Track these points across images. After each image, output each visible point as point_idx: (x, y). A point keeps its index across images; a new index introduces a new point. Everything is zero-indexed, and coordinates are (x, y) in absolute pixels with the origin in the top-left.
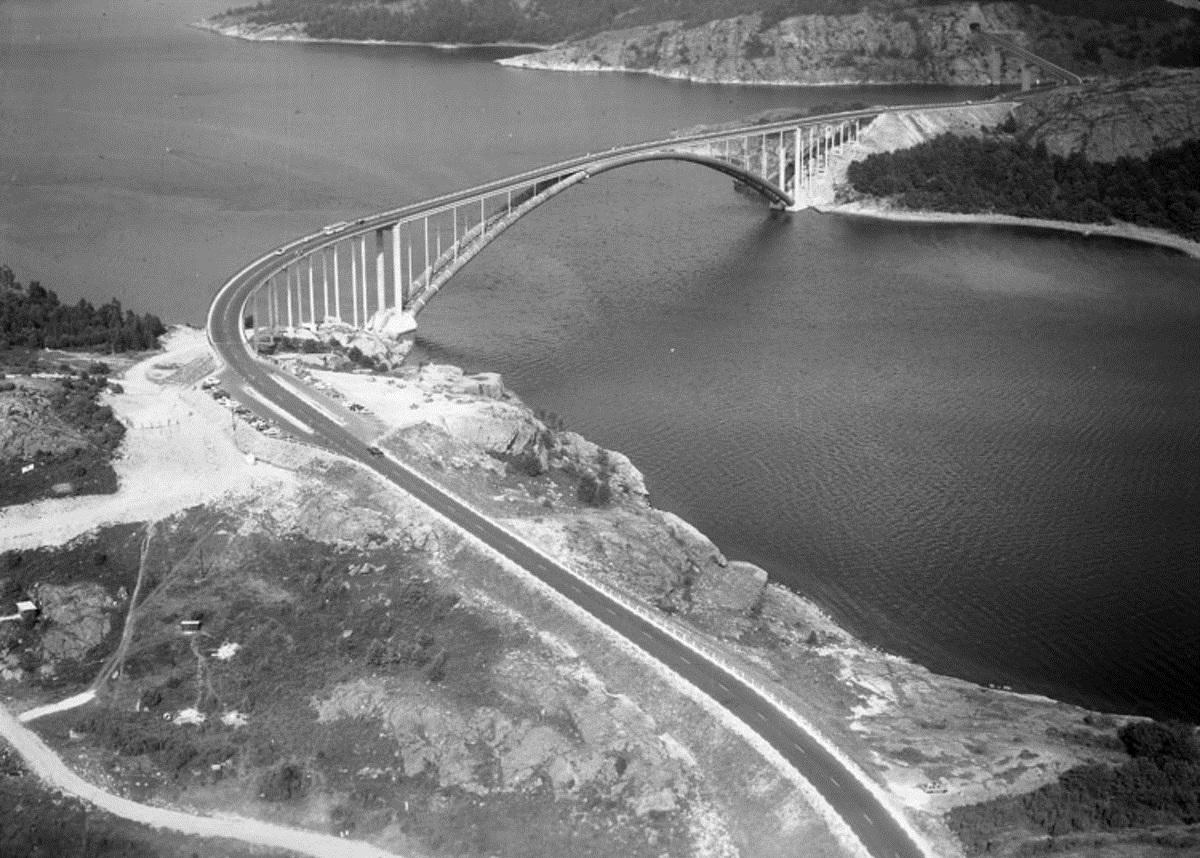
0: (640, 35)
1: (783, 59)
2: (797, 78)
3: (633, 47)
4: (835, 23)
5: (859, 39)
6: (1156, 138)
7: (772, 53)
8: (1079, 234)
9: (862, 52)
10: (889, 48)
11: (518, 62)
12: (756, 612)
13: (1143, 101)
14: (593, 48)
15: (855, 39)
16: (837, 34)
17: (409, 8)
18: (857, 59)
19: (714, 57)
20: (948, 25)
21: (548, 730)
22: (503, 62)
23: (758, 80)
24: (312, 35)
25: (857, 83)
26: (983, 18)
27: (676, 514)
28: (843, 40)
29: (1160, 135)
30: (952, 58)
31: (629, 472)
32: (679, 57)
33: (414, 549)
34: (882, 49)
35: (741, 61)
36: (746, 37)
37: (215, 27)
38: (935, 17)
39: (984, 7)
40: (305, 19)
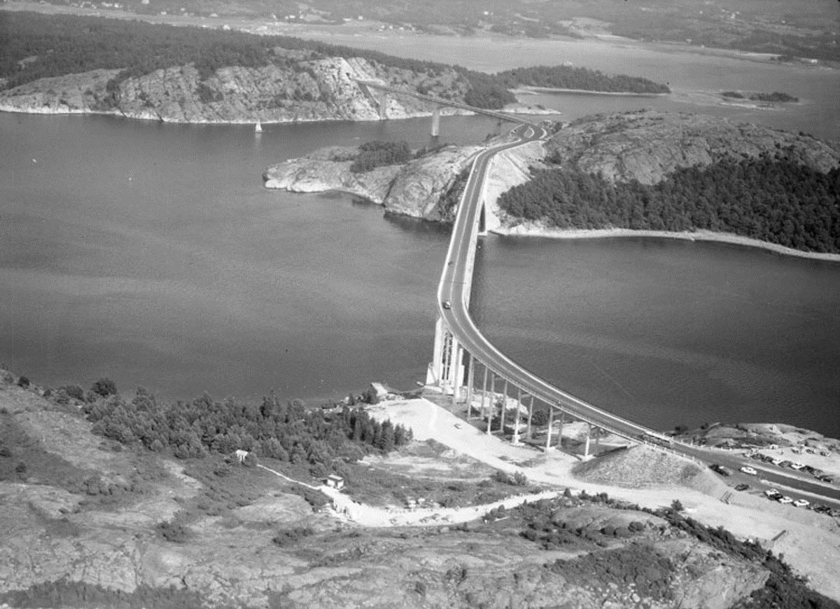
9: (284, 96)
15: (276, 85)
16: (262, 82)
19: (174, 101)
20: (336, 74)
25: (291, 120)
26: (351, 69)
30: (350, 100)
34: (297, 92)
39: (349, 60)
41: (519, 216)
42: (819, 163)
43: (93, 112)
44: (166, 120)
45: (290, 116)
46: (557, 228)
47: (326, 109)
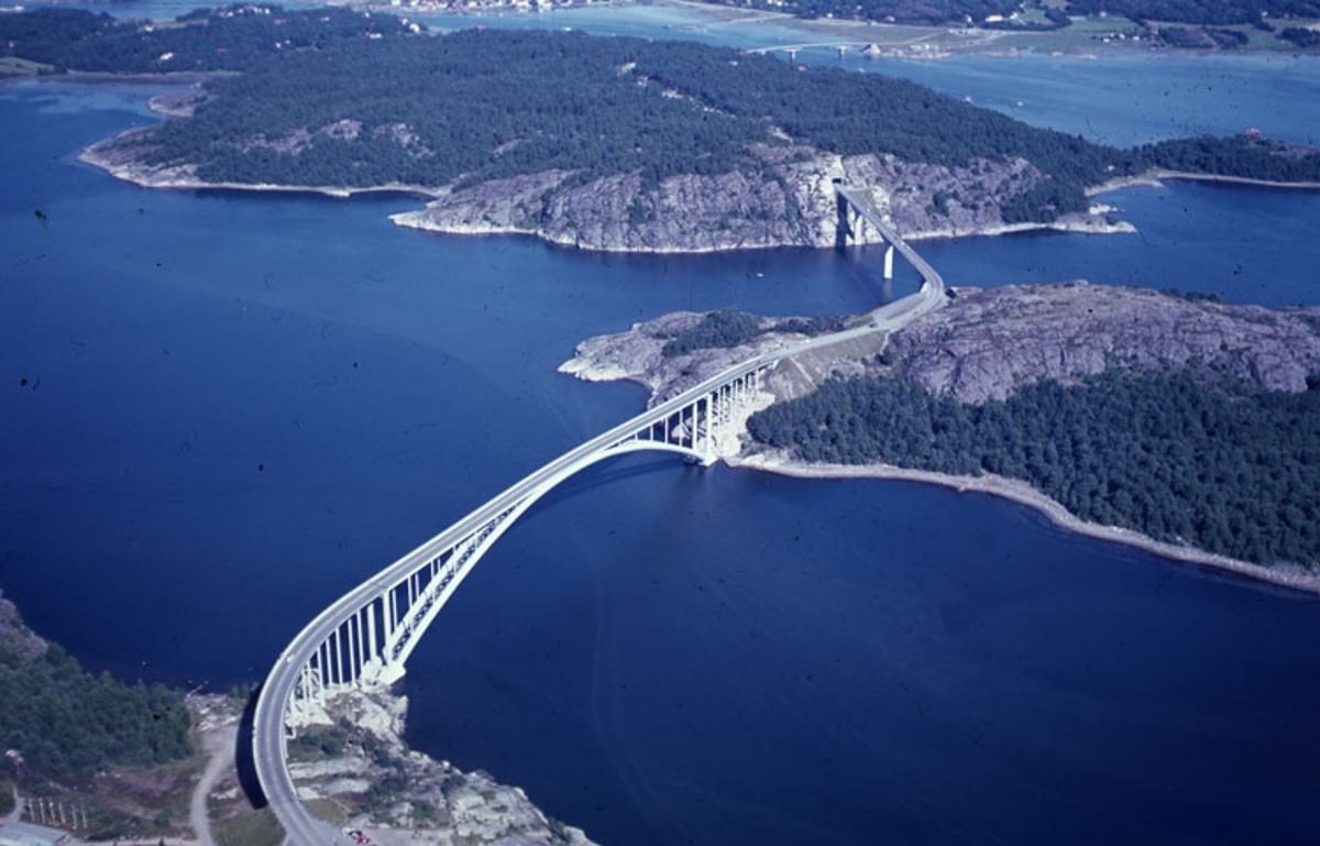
1: (664, 223)
2: (679, 244)
3: (520, 205)
4: (711, 184)
5: (733, 201)
6: (1015, 375)
7: (652, 217)
9: (735, 214)
13: (1003, 336)
14: (482, 205)
15: (729, 200)
18: (732, 221)
20: (813, 185)
22: (398, 219)
23: (643, 247)
24: (203, 179)
28: (723, 202)
29: (1019, 371)
30: (818, 219)
32: (566, 219)
34: (753, 209)
35: (626, 227)
36: (629, 201)
37: (104, 164)
38: (801, 175)
40: (197, 160)
41: (763, 442)
42: (1268, 376)
43: (519, 231)
44: (582, 245)
45: (733, 240)
46: (803, 460)
47: (784, 231)
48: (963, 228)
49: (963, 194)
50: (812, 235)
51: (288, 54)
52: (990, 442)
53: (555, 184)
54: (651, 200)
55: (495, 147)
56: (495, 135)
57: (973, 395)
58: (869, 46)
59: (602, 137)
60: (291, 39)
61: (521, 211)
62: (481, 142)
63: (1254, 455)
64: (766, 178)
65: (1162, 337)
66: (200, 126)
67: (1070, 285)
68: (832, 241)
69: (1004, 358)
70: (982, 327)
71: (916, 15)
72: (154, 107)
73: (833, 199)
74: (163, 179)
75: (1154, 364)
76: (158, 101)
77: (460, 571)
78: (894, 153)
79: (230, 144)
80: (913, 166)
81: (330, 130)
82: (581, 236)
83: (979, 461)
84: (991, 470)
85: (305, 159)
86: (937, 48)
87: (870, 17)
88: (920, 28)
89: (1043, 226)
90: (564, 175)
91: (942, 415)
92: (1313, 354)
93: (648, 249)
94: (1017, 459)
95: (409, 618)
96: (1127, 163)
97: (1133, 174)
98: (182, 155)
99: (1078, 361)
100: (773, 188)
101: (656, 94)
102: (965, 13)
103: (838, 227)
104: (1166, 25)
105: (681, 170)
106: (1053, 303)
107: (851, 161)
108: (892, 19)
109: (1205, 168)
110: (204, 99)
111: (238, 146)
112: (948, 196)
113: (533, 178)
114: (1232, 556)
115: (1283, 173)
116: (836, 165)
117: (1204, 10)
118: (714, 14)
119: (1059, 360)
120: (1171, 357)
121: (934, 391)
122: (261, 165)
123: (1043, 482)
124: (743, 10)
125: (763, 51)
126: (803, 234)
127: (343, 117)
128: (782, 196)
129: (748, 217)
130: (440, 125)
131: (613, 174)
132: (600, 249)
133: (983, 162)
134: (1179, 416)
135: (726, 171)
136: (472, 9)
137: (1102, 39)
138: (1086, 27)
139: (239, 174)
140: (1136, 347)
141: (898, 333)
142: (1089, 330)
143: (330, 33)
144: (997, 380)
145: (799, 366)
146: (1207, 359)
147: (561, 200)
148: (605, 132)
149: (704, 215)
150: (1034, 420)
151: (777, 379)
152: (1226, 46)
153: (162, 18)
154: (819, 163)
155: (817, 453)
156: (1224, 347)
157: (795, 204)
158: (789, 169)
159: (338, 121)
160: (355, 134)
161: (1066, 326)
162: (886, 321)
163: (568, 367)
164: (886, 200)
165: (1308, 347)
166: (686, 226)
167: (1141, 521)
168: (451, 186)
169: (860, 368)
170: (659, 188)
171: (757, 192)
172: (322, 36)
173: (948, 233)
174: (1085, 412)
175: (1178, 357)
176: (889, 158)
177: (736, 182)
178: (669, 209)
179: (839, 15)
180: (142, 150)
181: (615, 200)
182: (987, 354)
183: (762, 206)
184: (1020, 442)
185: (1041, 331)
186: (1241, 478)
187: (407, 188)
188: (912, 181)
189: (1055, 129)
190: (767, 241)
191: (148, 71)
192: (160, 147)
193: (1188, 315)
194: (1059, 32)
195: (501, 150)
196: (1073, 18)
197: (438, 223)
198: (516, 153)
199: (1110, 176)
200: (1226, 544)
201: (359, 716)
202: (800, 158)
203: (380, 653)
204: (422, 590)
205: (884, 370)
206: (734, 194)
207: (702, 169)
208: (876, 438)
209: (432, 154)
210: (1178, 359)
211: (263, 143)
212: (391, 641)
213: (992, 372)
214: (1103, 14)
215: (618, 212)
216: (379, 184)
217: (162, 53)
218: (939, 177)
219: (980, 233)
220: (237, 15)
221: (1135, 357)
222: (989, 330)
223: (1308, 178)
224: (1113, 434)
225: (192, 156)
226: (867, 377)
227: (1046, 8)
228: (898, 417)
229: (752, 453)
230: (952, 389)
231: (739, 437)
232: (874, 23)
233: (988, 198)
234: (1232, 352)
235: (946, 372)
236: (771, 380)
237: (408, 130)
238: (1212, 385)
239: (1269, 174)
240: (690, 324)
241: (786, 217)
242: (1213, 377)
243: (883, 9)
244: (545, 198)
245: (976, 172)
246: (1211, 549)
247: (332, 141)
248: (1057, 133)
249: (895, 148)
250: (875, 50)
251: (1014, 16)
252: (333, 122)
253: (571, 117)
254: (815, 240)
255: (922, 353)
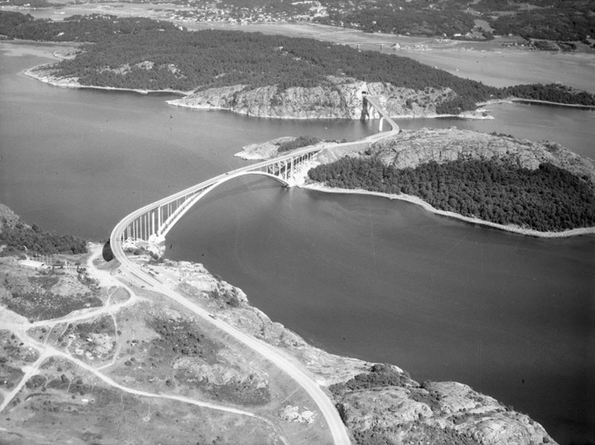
0: (227, 92)
2: (292, 116)
3: (223, 98)
4: (308, 91)
6: (420, 160)
7: (281, 104)
8: (388, 199)
9: (317, 104)
10: (329, 102)
11: (175, 102)
12: (282, 337)
13: (416, 145)
14: (207, 97)
15: (315, 98)
17: (124, 72)
20: (353, 93)
21: (232, 369)
22: (169, 102)
27: (258, 308)
28: (312, 98)
30: (354, 107)
31: (242, 295)
32: (243, 104)
33: (190, 322)
34: (326, 103)
35: (269, 107)
36: (271, 97)
37: (36, 76)
40: (79, 75)
41: (313, 179)
42: (523, 164)
43: (223, 108)
44: (250, 114)
45: (316, 115)
47: (339, 113)
48: (418, 114)
49: (420, 101)
50: (351, 114)
51: (120, 36)
52: (405, 182)
53: (239, 90)
54: (281, 97)
55: (214, 76)
56: (215, 71)
57: (401, 166)
58: (395, 44)
59: (263, 73)
60: (121, 30)
61: (224, 100)
62: (208, 74)
63: (509, 189)
64: (332, 90)
65: (483, 148)
66: (80, 61)
67: (449, 128)
68: (359, 117)
69: (416, 153)
70: (409, 141)
71: (420, 32)
72: (56, 55)
73: (361, 99)
74: (63, 83)
75: (478, 158)
76: (57, 53)
77: (188, 205)
78: (392, 83)
79: (94, 70)
80: (398, 89)
81: (140, 65)
82: (249, 111)
83: (400, 189)
84: (404, 192)
85: (128, 77)
86: (427, 47)
87: (399, 33)
88: (422, 38)
89: (454, 116)
90: (244, 86)
91: (388, 172)
92: (545, 157)
93: (278, 117)
94: (415, 189)
95: (167, 221)
96: (499, 94)
97: (500, 98)
98: (71, 73)
99: (447, 156)
100: (335, 94)
101: (290, 58)
102: (444, 32)
103: (362, 111)
104: (538, 40)
105: (295, 85)
106: (440, 134)
107: (371, 84)
108: (409, 34)
109: (533, 97)
110: (80, 52)
111: (97, 70)
112: (413, 101)
113: (230, 87)
114: (492, 221)
115: (568, 100)
116: (364, 86)
117: (559, 34)
118: (325, 29)
119: (439, 155)
120: (485, 156)
121: (387, 165)
122: (109, 78)
123: (424, 196)
124: (339, 28)
125: (344, 44)
126: (347, 114)
127: (146, 60)
128: (339, 97)
129: (323, 106)
130: (190, 66)
131: (265, 86)
132: (258, 116)
133: (431, 89)
134: (482, 174)
135: (315, 86)
136: (210, 22)
137: (507, 46)
138: (501, 40)
139: (98, 82)
140: (471, 151)
141: (375, 143)
142: (453, 144)
143: (140, 28)
144: (412, 160)
145: (332, 152)
146: (500, 157)
147: (242, 95)
148: (264, 71)
149: (304, 104)
150: (424, 175)
151: (322, 157)
152: (565, 50)
153: (58, 16)
154: (356, 84)
155: (335, 184)
156: (508, 153)
157: (345, 101)
158: (343, 86)
159: (144, 61)
160: (151, 67)
161: (443, 142)
162: (371, 140)
163: (239, 154)
164: (385, 101)
165: (543, 155)
166: (296, 108)
167: (459, 209)
168: (194, 91)
169: (357, 155)
170: (285, 92)
171: (328, 95)
172: (136, 29)
173: (411, 116)
174: (445, 172)
175: (488, 156)
176: (388, 84)
177: (319, 90)
178: (289, 101)
179: (384, 31)
180: (53, 71)
181: (265, 96)
182: (409, 151)
183: (330, 101)
184: (417, 182)
185: (432, 143)
186: (501, 196)
187: (174, 91)
188: (398, 94)
189: (470, 79)
190: (330, 116)
191: (53, 40)
192: (61, 70)
193: (495, 140)
194: (487, 42)
195: (217, 77)
196: (495, 36)
197: (187, 104)
198: (223, 78)
199: (490, 99)
200: (490, 218)
201: (147, 247)
202: (348, 82)
203: (156, 233)
204: (173, 212)
205: (367, 157)
206: (318, 96)
207: (305, 85)
208: (360, 180)
209: (185, 78)
210: (488, 157)
211: (109, 69)
212: (160, 229)
213: (410, 158)
214: (510, 35)
215: (266, 101)
216: (161, 89)
217: (59, 32)
218: (409, 93)
219: (425, 117)
220: (94, 19)
221: (470, 155)
222: (412, 142)
223: (578, 103)
224: (454, 180)
225: (76, 74)
226: (360, 158)
227: (483, 31)
228: (370, 172)
229: (310, 183)
230: (394, 164)
231: (305, 178)
232: (400, 36)
233: (431, 103)
234: (511, 155)
235: (392, 157)
236: (320, 157)
237: (175, 67)
238: (500, 166)
239: (561, 100)
240: (291, 140)
241: (340, 106)
242: (501, 163)
243: (405, 29)
244: (235, 96)
245: (427, 93)
246: (484, 219)
247: (141, 70)
248: (471, 81)
249: (392, 80)
250: (398, 46)
251: (468, 34)
252: (141, 62)
253: (250, 65)
254: (352, 116)
255: (383, 150)
